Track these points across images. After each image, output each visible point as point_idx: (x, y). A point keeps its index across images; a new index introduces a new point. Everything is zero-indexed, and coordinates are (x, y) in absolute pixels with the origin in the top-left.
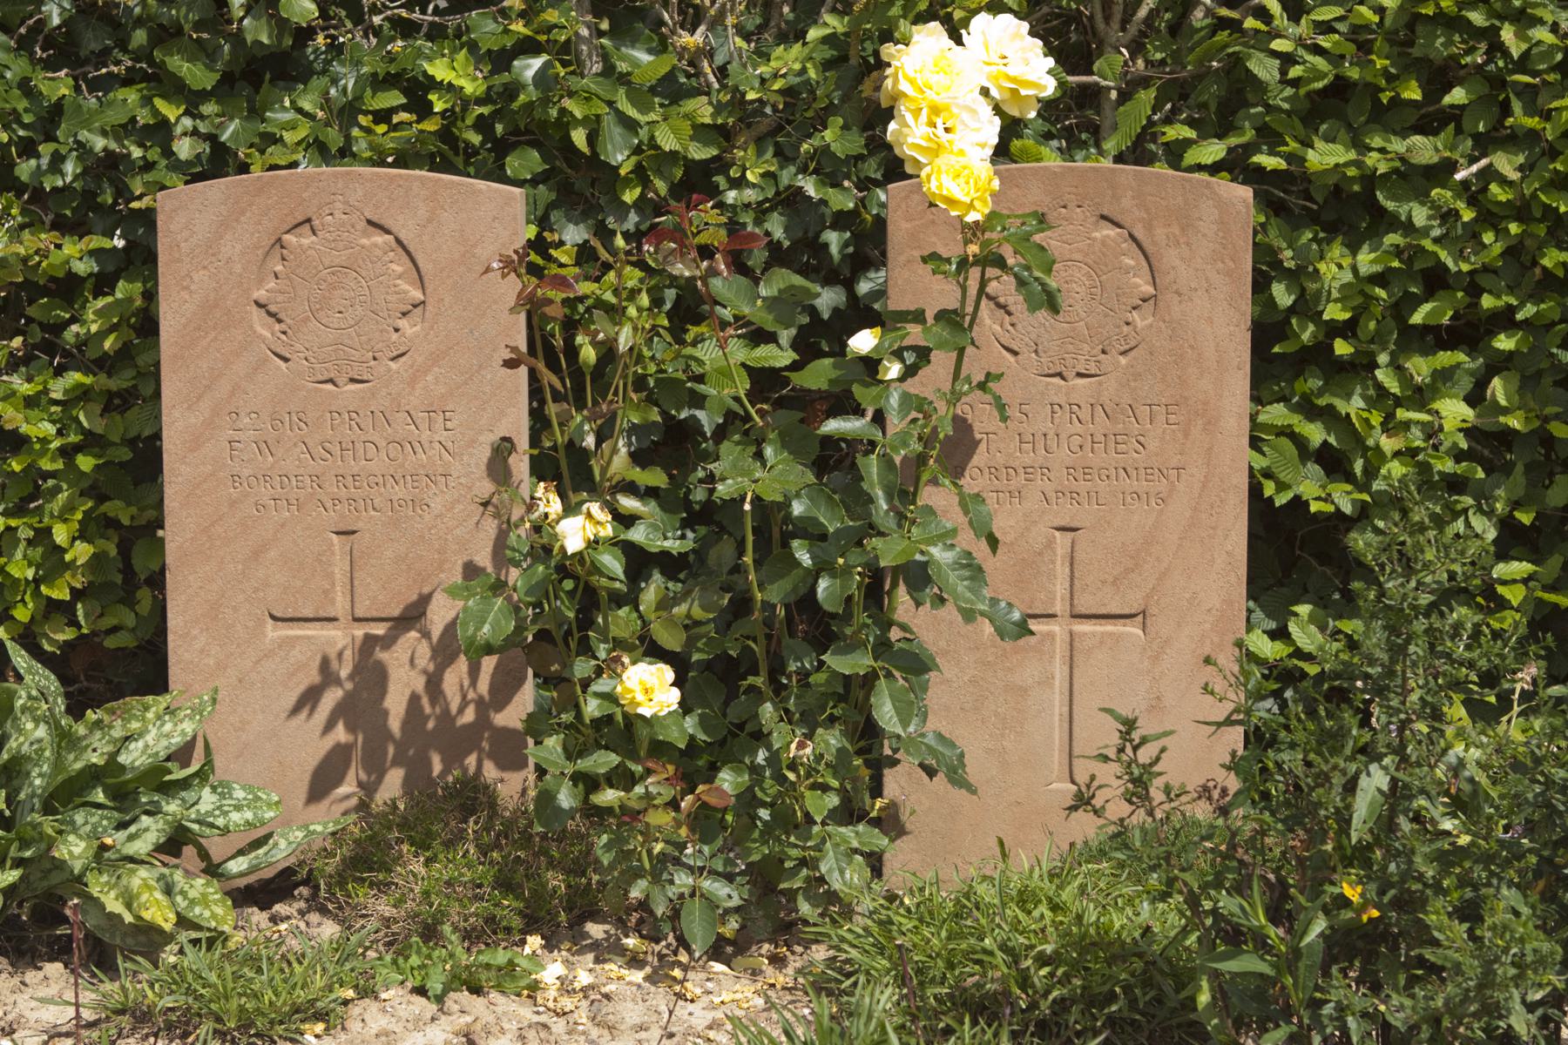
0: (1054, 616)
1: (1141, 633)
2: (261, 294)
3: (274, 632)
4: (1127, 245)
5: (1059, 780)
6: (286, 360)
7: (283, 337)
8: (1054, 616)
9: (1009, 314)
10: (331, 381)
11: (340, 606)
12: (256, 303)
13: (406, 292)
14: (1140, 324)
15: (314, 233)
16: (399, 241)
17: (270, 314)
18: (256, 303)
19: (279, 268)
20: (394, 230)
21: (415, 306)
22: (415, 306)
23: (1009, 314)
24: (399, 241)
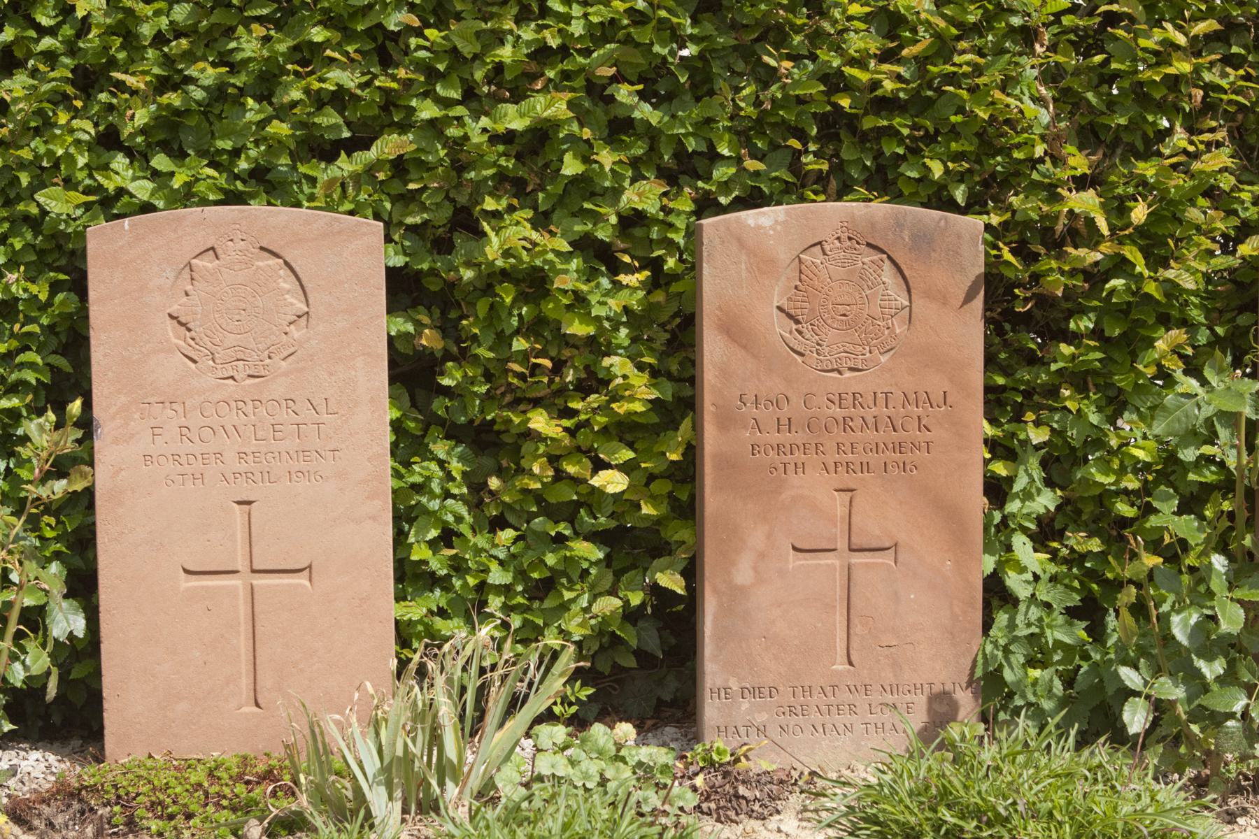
0: (237, 572)
1: (307, 583)
2: (174, 309)
3: (795, 561)
4: (284, 272)
5: (247, 704)
6: (194, 361)
7: (192, 343)
8: (237, 572)
9: (189, 330)
10: (232, 377)
11: (241, 564)
12: (170, 316)
13: (292, 304)
14: (296, 335)
15: (217, 258)
16: (286, 263)
17: (180, 323)
18: (170, 316)
19: (189, 288)
20: (282, 254)
21: (299, 317)
22: (299, 317)
23: (189, 330)
24: (286, 263)
